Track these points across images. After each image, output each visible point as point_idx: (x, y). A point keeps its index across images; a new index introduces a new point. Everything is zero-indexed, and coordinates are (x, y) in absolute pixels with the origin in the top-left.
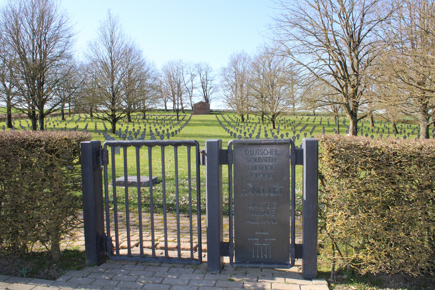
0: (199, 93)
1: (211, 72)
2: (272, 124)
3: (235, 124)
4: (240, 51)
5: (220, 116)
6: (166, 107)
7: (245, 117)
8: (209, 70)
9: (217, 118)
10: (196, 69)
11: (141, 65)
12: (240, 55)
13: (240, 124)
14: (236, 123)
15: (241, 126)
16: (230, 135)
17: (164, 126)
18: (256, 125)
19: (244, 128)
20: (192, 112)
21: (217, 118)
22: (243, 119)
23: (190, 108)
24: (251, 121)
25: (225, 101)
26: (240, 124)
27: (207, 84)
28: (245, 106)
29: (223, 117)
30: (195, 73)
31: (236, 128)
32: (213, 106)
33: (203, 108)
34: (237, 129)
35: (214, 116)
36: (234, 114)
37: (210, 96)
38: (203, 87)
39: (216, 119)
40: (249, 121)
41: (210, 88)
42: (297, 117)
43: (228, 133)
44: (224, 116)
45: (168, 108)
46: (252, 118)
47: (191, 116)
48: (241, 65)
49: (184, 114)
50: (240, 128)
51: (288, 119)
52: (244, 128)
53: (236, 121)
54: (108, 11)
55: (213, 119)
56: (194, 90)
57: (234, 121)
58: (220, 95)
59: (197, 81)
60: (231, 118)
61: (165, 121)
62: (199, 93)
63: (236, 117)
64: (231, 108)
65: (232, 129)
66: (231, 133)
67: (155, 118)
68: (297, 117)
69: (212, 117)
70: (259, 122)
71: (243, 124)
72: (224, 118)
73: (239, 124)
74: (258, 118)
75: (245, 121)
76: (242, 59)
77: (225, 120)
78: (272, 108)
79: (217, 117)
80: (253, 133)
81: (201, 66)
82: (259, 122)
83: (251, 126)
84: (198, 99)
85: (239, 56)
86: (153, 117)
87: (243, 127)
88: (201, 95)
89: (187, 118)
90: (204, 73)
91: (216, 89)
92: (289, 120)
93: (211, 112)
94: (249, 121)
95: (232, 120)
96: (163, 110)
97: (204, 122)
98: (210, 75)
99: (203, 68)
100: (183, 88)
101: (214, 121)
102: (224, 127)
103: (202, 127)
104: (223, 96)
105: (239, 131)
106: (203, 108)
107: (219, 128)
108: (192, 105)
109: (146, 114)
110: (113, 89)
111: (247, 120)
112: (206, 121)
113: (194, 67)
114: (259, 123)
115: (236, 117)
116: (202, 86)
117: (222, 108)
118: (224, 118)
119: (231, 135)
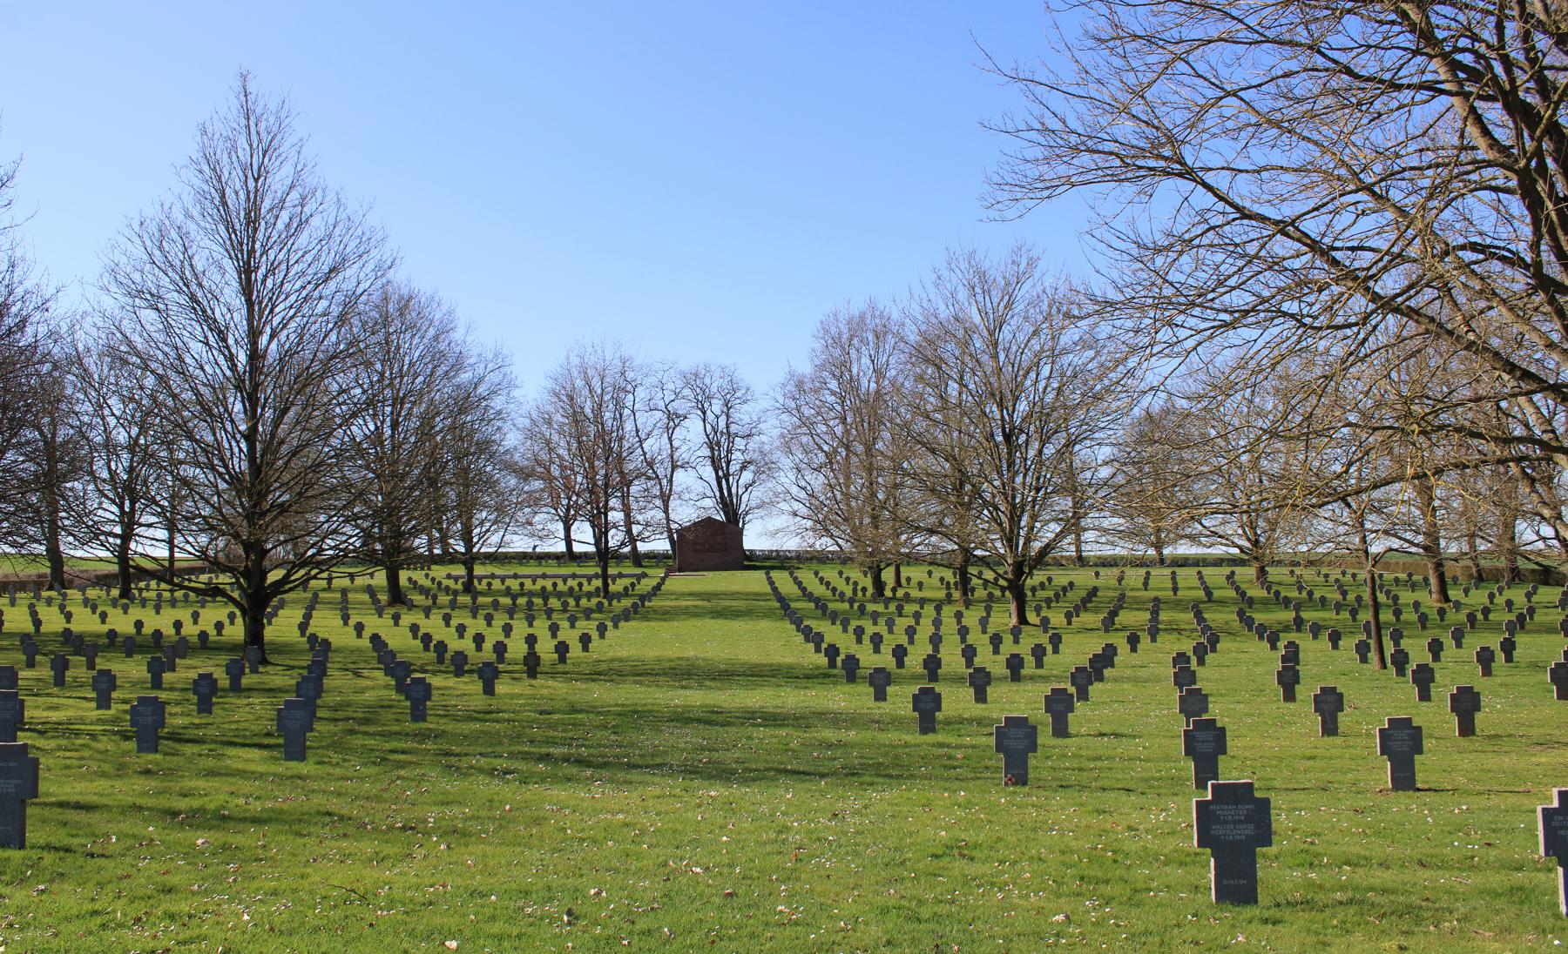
0: (699, 487)
1: (745, 402)
2: (1013, 607)
3: (846, 606)
4: (858, 306)
5: (786, 574)
6: (568, 541)
7: (888, 575)
8: (738, 394)
9: (772, 583)
10: (687, 392)
11: (443, 360)
12: (862, 317)
13: (870, 607)
14: (851, 601)
15: (875, 616)
16: (822, 660)
17: (573, 621)
18: (938, 609)
19: (890, 624)
20: (670, 562)
21: (772, 583)
22: (879, 585)
23: (662, 545)
24: (915, 593)
25: (804, 511)
26: (870, 607)
27: (729, 451)
28: (885, 528)
29: (795, 579)
30: (680, 406)
31: (854, 623)
32: (754, 539)
33: (713, 543)
34: (859, 632)
35: (761, 574)
36: (840, 567)
37: (745, 498)
38: (713, 462)
39: (768, 589)
40: (907, 595)
41: (743, 468)
42: (1097, 574)
43: (818, 650)
44: (798, 574)
45: (577, 548)
46: (914, 582)
47: (663, 579)
48: (865, 361)
49: (639, 571)
50: (870, 629)
51: (1064, 581)
52: (890, 624)
53: (849, 592)
54: (237, 84)
55: (757, 589)
56: (679, 475)
57: (842, 594)
58: (780, 489)
59: (692, 434)
60: (828, 584)
61: (578, 599)
62: (699, 487)
63: (848, 579)
64: (825, 544)
65: (832, 633)
66: (832, 652)
67: (550, 588)
68: (1097, 574)
69: (753, 581)
70: (949, 595)
71: (880, 608)
72: (799, 584)
73: (862, 609)
74: (942, 579)
75: (888, 593)
76: (871, 337)
77: (804, 590)
78: (1010, 540)
79: (769, 578)
80: (911, 642)
81: (707, 381)
82: (949, 595)
83: (917, 616)
84: (693, 499)
85: (857, 326)
86: (540, 583)
87: (882, 621)
88: (709, 493)
89: (646, 585)
90: (717, 406)
91: (763, 467)
92: (1071, 584)
93: (749, 561)
94: (907, 595)
95: (834, 590)
96: (557, 557)
97: (714, 602)
98: (744, 415)
99: (714, 389)
100: (634, 462)
101: (757, 596)
102: (797, 620)
103: (699, 623)
104: (794, 490)
105: (866, 639)
106: (713, 543)
107: (779, 624)
108: (670, 531)
109: (479, 570)
110: (252, 448)
111: (894, 590)
112: (733, 595)
113: (679, 384)
114: (949, 599)
115: (848, 579)
116: (712, 458)
117: (791, 544)
118: (799, 584)
119: (832, 664)
